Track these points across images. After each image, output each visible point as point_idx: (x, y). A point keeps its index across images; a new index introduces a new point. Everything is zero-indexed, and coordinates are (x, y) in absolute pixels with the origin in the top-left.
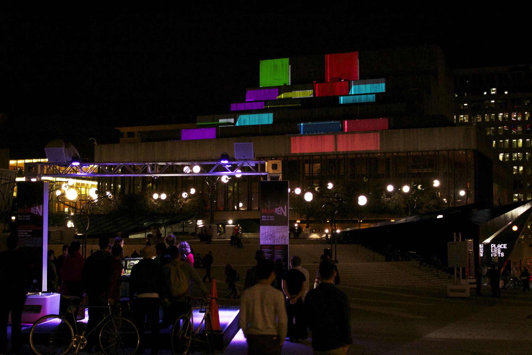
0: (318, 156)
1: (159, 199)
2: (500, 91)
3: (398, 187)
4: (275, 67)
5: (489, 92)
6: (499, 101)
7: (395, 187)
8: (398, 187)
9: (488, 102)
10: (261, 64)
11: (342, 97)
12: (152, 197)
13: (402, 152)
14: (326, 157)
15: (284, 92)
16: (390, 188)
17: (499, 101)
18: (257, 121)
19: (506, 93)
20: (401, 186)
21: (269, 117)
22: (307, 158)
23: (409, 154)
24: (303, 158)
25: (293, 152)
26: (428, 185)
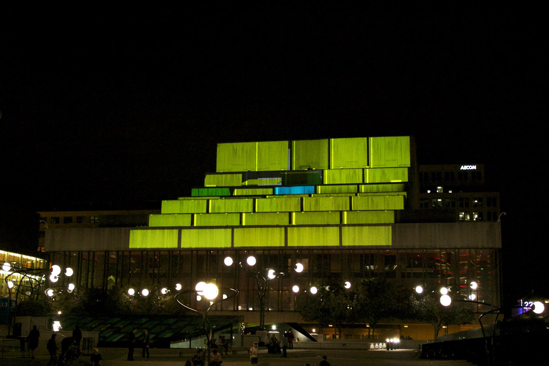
0: (316, 250)
1: (477, 291)
2: (446, 190)
3: (139, 290)
4: (235, 152)
5: (434, 190)
6: (447, 200)
7: (300, 288)
8: (139, 290)
9: (435, 200)
10: (218, 148)
11: (320, 187)
12: (127, 293)
13: (417, 249)
14: (123, 253)
15: (249, 178)
16: (131, 292)
17: (447, 200)
18: (234, 208)
19: (450, 192)
20: (140, 290)
21: (248, 205)
22: (307, 252)
23: (311, 251)
24: (160, 253)
25: (131, 246)
26: (338, 288)
